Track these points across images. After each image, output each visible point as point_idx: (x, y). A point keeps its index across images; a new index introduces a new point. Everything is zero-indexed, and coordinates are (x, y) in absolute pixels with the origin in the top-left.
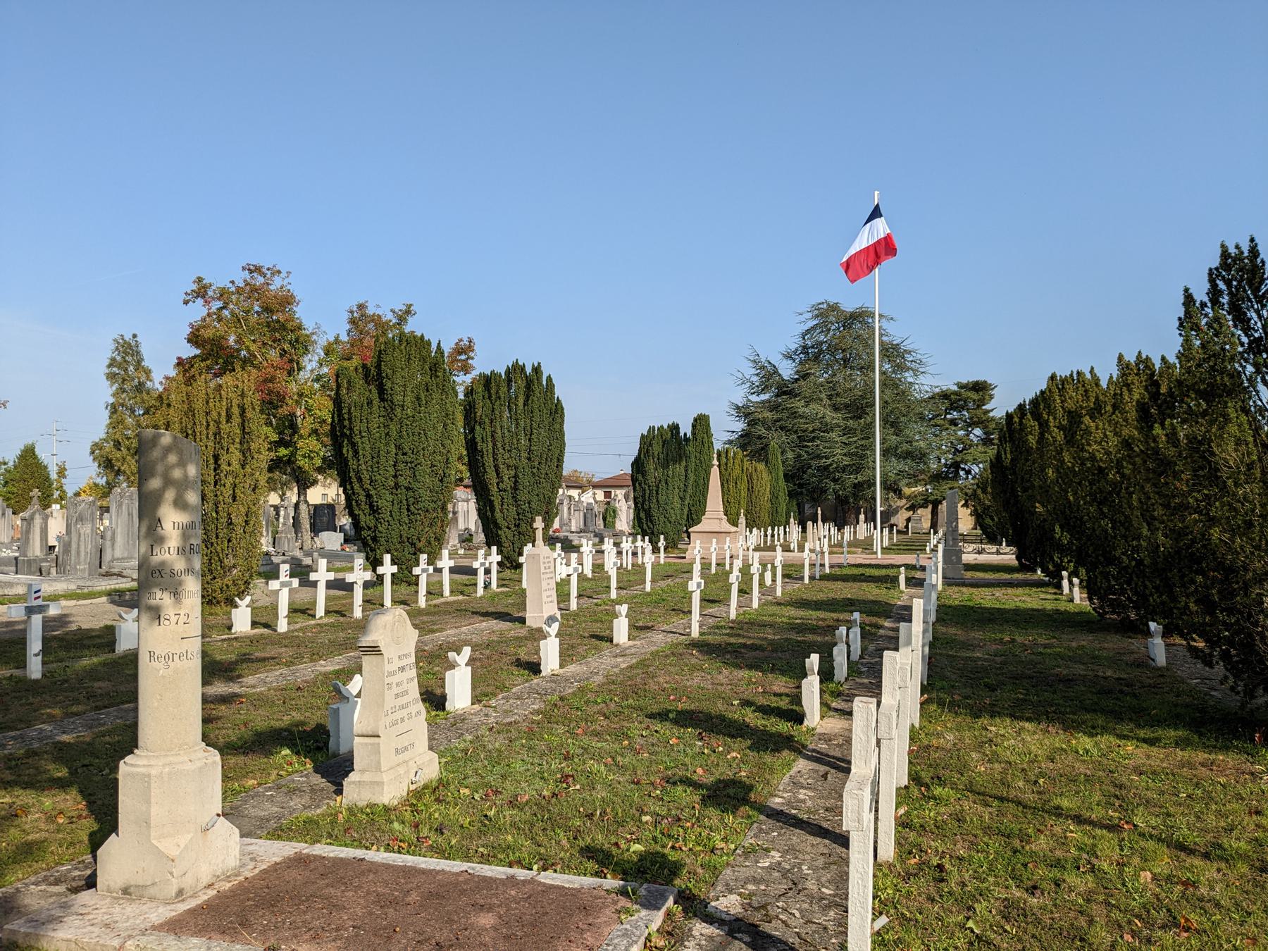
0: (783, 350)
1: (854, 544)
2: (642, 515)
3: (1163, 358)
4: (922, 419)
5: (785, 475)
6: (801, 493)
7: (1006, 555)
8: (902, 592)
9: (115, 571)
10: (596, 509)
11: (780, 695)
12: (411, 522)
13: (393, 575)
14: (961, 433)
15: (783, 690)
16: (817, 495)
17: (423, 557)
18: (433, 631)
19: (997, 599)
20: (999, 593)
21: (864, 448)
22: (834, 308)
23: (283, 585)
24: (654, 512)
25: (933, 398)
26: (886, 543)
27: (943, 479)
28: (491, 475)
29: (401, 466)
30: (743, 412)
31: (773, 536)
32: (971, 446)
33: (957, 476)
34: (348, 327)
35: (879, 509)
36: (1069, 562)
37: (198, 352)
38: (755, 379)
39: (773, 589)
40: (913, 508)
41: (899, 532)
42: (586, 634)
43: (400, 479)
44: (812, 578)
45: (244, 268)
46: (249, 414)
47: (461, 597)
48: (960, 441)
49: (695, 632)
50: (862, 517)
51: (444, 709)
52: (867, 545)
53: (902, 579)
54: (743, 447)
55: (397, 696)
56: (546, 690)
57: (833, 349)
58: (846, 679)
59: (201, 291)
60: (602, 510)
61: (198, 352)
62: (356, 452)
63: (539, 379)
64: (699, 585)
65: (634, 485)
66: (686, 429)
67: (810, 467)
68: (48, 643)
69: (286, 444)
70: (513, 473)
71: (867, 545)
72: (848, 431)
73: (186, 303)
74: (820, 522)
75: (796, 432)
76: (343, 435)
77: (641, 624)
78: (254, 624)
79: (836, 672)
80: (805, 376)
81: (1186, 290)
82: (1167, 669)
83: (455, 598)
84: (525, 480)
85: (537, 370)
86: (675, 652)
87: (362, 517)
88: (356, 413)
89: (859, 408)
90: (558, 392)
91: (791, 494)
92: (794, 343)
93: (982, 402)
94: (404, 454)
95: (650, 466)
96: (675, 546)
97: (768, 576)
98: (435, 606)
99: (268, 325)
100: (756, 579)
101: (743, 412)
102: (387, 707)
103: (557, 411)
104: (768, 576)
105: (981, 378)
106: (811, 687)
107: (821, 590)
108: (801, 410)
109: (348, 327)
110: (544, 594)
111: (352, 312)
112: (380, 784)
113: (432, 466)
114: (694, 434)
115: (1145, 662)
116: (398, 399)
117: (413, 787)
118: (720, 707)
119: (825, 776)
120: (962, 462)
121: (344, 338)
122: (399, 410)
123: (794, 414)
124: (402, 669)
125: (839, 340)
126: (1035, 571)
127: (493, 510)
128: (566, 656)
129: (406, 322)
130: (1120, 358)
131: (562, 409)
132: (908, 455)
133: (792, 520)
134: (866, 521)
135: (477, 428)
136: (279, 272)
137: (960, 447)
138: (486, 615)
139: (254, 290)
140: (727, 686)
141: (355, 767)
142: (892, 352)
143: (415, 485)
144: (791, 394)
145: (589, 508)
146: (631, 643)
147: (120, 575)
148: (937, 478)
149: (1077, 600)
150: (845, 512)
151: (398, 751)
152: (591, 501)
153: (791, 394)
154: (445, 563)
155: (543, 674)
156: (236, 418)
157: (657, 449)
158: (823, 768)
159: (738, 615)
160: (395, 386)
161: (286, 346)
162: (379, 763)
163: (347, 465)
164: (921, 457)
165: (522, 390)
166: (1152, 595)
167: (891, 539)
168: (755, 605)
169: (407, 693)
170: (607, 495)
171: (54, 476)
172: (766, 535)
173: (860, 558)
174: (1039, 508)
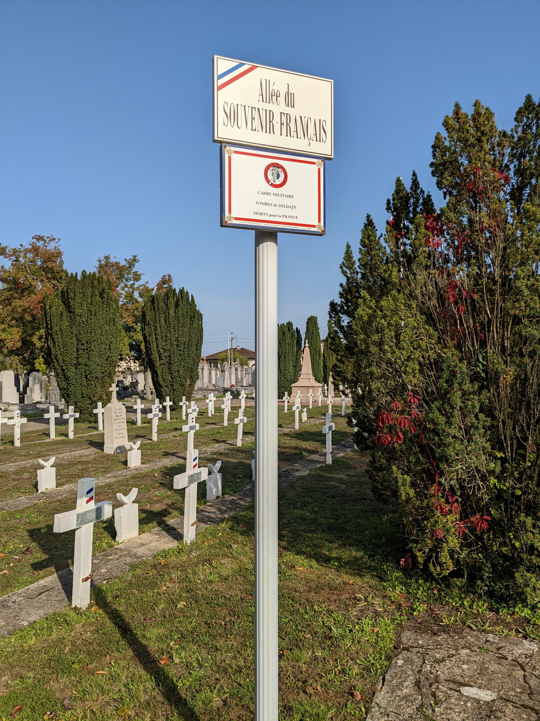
13: (56, 418)
45: (33, 238)
62: (54, 343)
68: (333, 406)
70: (167, 354)
84: (175, 359)
94: (82, 344)
103: (195, 317)
111: (100, 261)
116: (78, 311)
127: (157, 376)
129: (134, 266)
136: (54, 239)
143: (89, 363)
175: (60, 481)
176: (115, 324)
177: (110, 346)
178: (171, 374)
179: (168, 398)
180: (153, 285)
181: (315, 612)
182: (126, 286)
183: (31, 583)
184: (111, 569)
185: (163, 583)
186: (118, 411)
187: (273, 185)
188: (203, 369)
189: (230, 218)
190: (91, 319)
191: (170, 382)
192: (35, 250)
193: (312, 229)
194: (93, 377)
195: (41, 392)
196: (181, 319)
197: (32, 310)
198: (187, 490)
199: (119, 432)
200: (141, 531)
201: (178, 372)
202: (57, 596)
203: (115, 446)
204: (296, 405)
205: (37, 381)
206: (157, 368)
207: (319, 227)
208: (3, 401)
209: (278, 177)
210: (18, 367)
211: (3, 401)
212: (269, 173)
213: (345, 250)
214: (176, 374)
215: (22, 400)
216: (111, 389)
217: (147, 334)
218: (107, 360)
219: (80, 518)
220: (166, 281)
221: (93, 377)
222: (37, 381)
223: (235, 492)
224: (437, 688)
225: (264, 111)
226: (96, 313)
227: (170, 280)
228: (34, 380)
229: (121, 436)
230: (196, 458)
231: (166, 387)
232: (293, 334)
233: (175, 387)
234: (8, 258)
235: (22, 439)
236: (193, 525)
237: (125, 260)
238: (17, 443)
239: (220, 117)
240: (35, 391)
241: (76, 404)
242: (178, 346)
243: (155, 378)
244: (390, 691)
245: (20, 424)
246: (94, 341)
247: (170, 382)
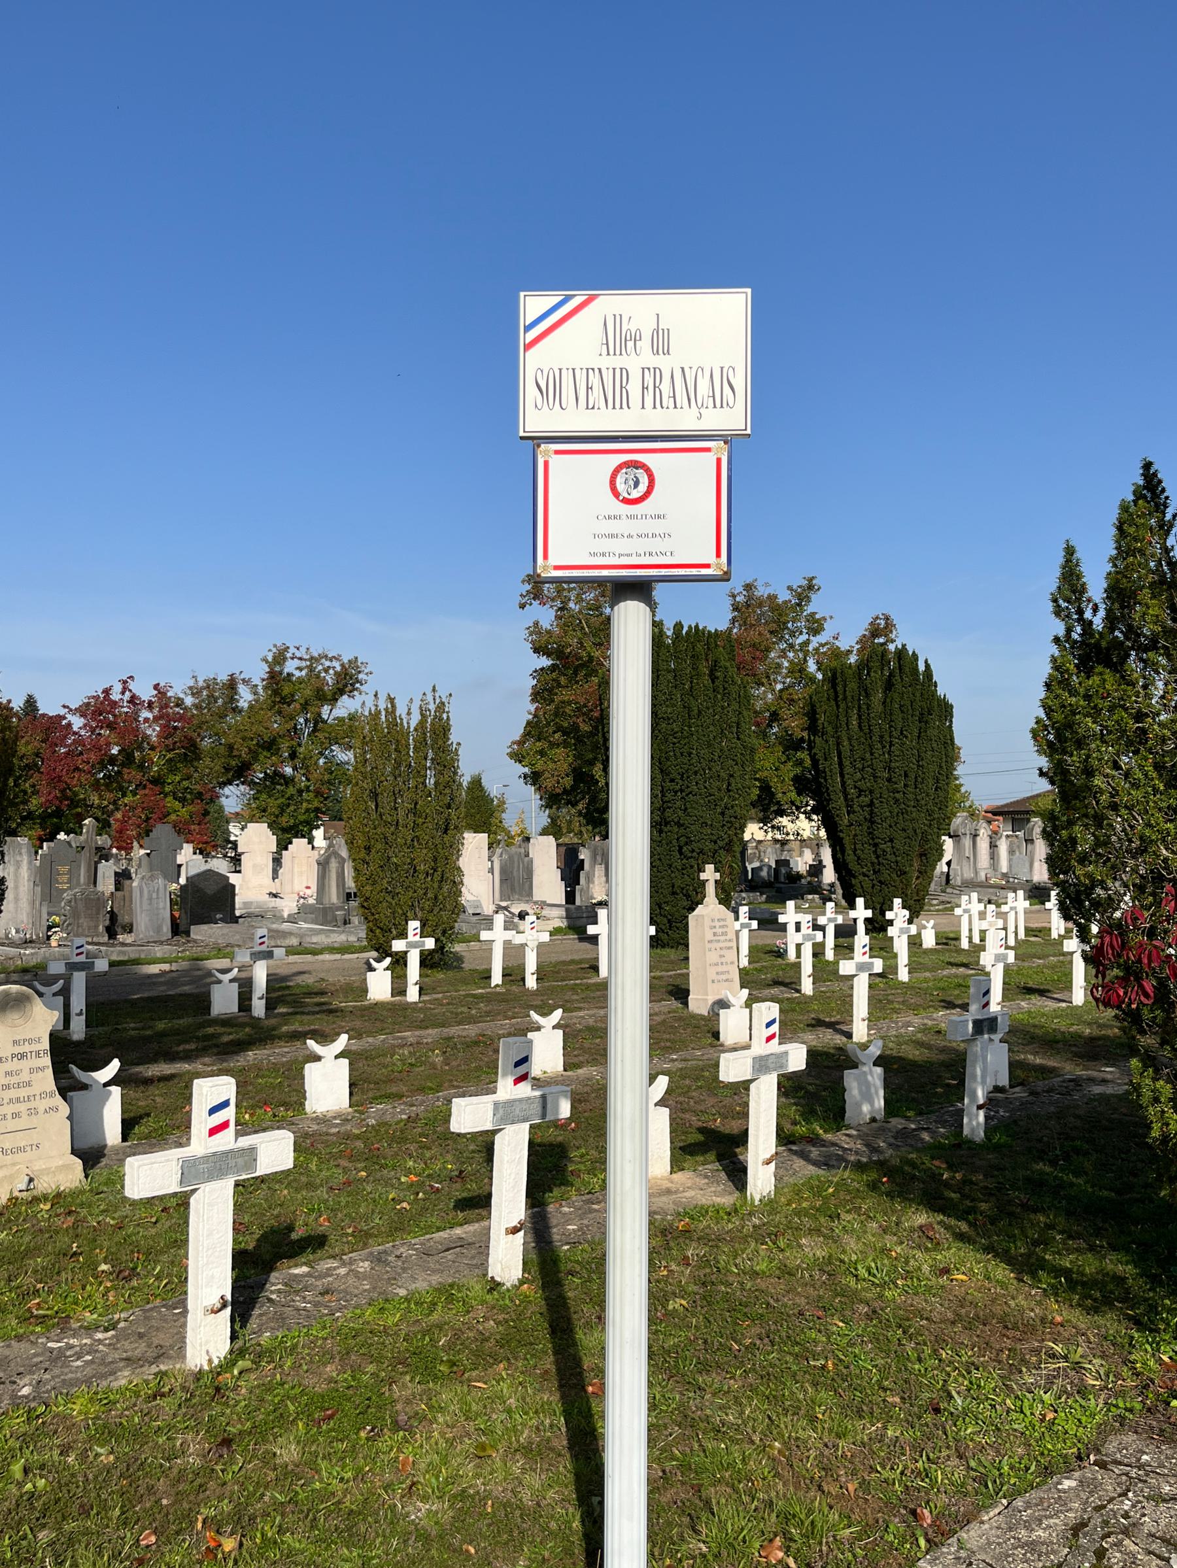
0: (37, 697)
70: (866, 800)
73: (522, 606)
81: (1147, 466)
84: (883, 810)
94: (672, 781)
111: (734, 596)
127: (843, 851)
129: (809, 600)
143: (686, 821)
175: (576, 1060)
176: (742, 737)
177: (729, 784)
178: (876, 845)
179: (860, 902)
180: (849, 640)
181: (940, 1360)
182: (791, 646)
183: (439, 1229)
184: (587, 1226)
185: (664, 1263)
186: (717, 924)
187: (627, 501)
188: (976, 835)
189: (545, 568)
190: (690, 727)
191: (872, 863)
193: (704, 571)
194: (693, 851)
196: (898, 717)
197: (592, 711)
198: (753, 1087)
199: (720, 969)
200: (676, 1165)
201: (891, 841)
202: (473, 1258)
206: (841, 831)
207: (718, 566)
208: (535, 899)
209: (636, 484)
210: (583, 829)
211: (535, 899)
212: (619, 480)
213: (1062, 560)
214: (887, 847)
215: (570, 897)
216: (703, 876)
217: (820, 756)
218: (723, 814)
219: (501, 1111)
220: (881, 629)
221: (693, 851)
222: (599, 858)
223: (920, 1114)
224: (1118, 1544)
225: (611, 371)
226: (700, 712)
227: (889, 625)
229: (724, 977)
230: (773, 1021)
231: (865, 875)
233: (885, 875)
234: (547, 606)
235: (541, 976)
236: (768, 1162)
237: (790, 588)
238: (531, 982)
239: (529, 394)
240: (596, 880)
242: (889, 780)
243: (839, 855)
244: (1004, 1526)
245: (536, 943)
246: (696, 773)
247: (872, 863)
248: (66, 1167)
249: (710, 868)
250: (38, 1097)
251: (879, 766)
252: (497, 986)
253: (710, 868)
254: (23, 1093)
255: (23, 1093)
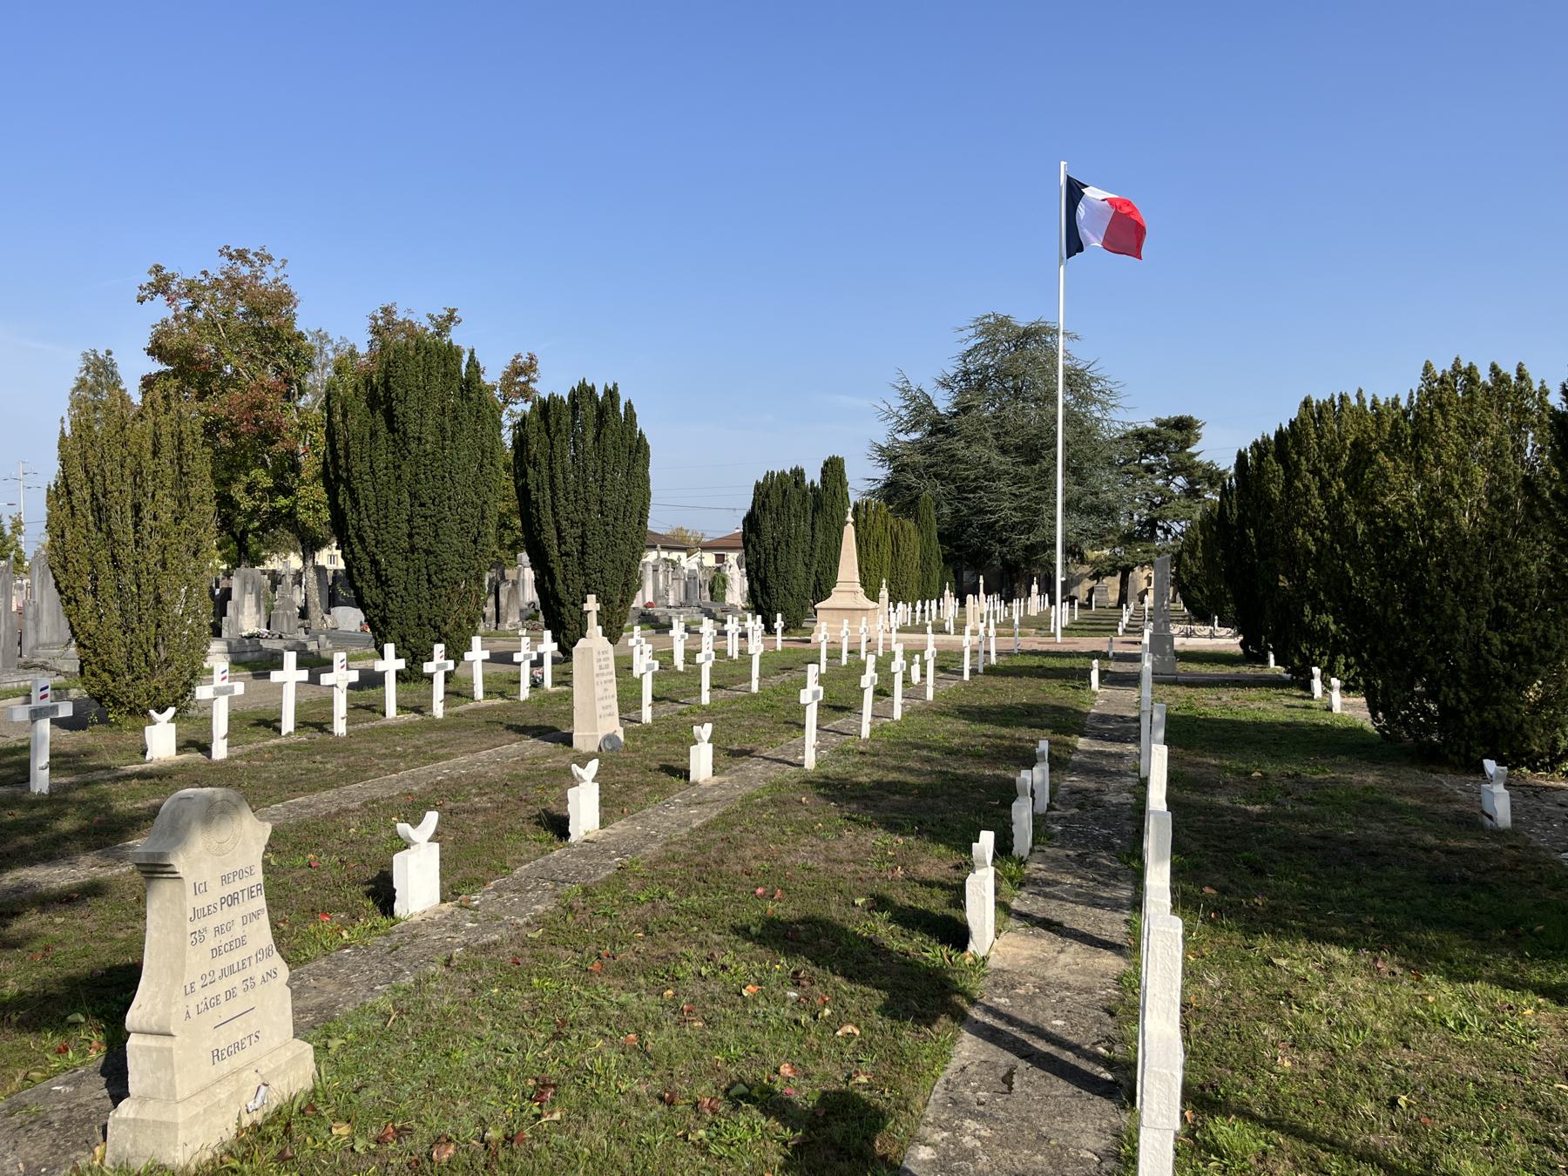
1: (1026, 622)
2: (757, 586)
3: (1494, 368)
4: (1111, 464)
5: (940, 535)
6: (960, 557)
7: (1227, 640)
8: (1095, 694)
9: (37, 661)
10: (700, 576)
11: (930, 884)
12: (433, 597)
13: (398, 672)
14: (1160, 482)
15: (934, 875)
16: (978, 560)
17: (439, 649)
18: (436, 759)
19: (1225, 706)
20: (1226, 695)
21: (1038, 500)
22: (1003, 322)
23: (219, 692)
24: (772, 582)
25: (1125, 438)
26: (1066, 622)
27: (1136, 540)
28: (550, 533)
29: (418, 521)
30: (888, 455)
31: (923, 611)
32: (1171, 498)
33: (1153, 536)
34: (370, 337)
35: (1059, 579)
36: (1321, 655)
37: (163, 367)
38: (903, 412)
39: (922, 687)
40: (1097, 576)
41: (1081, 606)
42: (655, 765)
43: (417, 539)
44: (974, 672)
46: (188, 448)
47: (499, 701)
48: (1159, 492)
49: (810, 760)
50: (1035, 588)
51: (392, 913)
52: (1041, 624)
53: (1095, 676)
54: (888, 500)
55: (216, 952)
56: (566, 872)
57: (1001, 374)
58: (1032, 851)
59: (161, 285)
60: (709, 578)
61: (163, 367)
62: (356, 502)
63: (615, 406)
64: (815, 695)
65: (745, 547)
66: (813, 476)
67: (971, 525)
69: (288, 492)
70: (579, 531)
71: (1041, 624)
72: (1019, 480)
73: (141, 300)
74: (982, 594)
75: (954, 481)
76: (338, 478)
77: (735, 747)
78: (180, 749)
79: (1015, 841)
80: (965, 410)
82: (1513, 832)
83: (489, 702)
84: (595, 542)
85: (612, 394)
86: (779, 799)
87: (366, 590)
88: (355, 448)
89: (1034, 450)
90: (642, 424)
91: (947, 559)
92: (952, 368)
93: (1187, 443)
94: (422, 505)
95: (767, 524)
96: (798, 626)
97: (916, 671)
98: (458, 715)
99: (256, 333)
100: (898, 679)
101: (888, 455)
102: (192, 975)
103: (638, 450)
104: (916, 671)
105: (1186, 414)
106: (981, 889)
107: (986, 692)
108: (960, 453)
109: (370, 337)
110: (599, 705)
112: (171, 1127)
113: (462, 521)
114: (823, 482)
115: (1473, 820)
116: (412, 429)
117: (247, 1121)
118: (834, 911)
119: (1008, 1080)
120: (1159, 518)
121: (363, 349)
122: (413, 446)
123: (952, 458)
124: (232, 900)
125: (1012, 363)
126: (1266, 662)
127: (553, 581)
128: (610, 807)
129: (447, 329)
130: (1427, 368)
131: (647, 447)
132: (1093, 510)
133: (947, 592)
134: (1039, 594)
135: (530, 471)
137: (1158, 500)
138: (523, 730)
139: (237, 285)
140: (855, 866)
141: (131, 1089)
142: (1075, 380)
143: (438, 548)
144: (948, 432)
145: (692, 576)
146: (716, 779)
147: (43, 667)
148: (1128, 539)
149: (1337, 709)
150: (1013, 581)
151: (217, 1055)
152: (695, 567)
153: (948, 432)
154: (477, 653)
155: (572, 839)
156: (168, 453)
157: (775, 500)
158: (1006, 1058)
159: (873, 731)
160: (406, 409)
161: (282, 361)
162: (172, 1084)
163: (344, 519)
164: (1111, 512)
165: (592, 421)
166: (1468, 712)
167: (1071, 614)
168: (897, 715)
169: (242, 942)
170: (720, 559)
171: (8, 532)
172: (914, 611)
173: (1033, 642)
174: (1284, 582)
177: (483, 512)
192: (236, 286)
195: (259, 611)
203: (601, 735)
204: (705, 651)
205: (249, 588)
222: (249, 588)
228: (244, 584)
232: (805, 495)
237: (431, 317)
241: (403, 640)
243: (548, 585)
248: (297, 1059)
249: (591, 598)
250: (253, 960)
251: (593, 499)
252: (289, 734)
253: (591, 598)
254: (236, 957)
255: (236, 957)
